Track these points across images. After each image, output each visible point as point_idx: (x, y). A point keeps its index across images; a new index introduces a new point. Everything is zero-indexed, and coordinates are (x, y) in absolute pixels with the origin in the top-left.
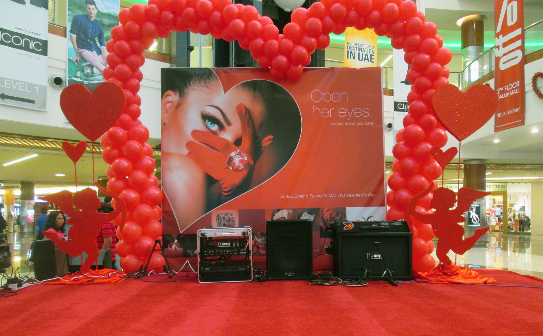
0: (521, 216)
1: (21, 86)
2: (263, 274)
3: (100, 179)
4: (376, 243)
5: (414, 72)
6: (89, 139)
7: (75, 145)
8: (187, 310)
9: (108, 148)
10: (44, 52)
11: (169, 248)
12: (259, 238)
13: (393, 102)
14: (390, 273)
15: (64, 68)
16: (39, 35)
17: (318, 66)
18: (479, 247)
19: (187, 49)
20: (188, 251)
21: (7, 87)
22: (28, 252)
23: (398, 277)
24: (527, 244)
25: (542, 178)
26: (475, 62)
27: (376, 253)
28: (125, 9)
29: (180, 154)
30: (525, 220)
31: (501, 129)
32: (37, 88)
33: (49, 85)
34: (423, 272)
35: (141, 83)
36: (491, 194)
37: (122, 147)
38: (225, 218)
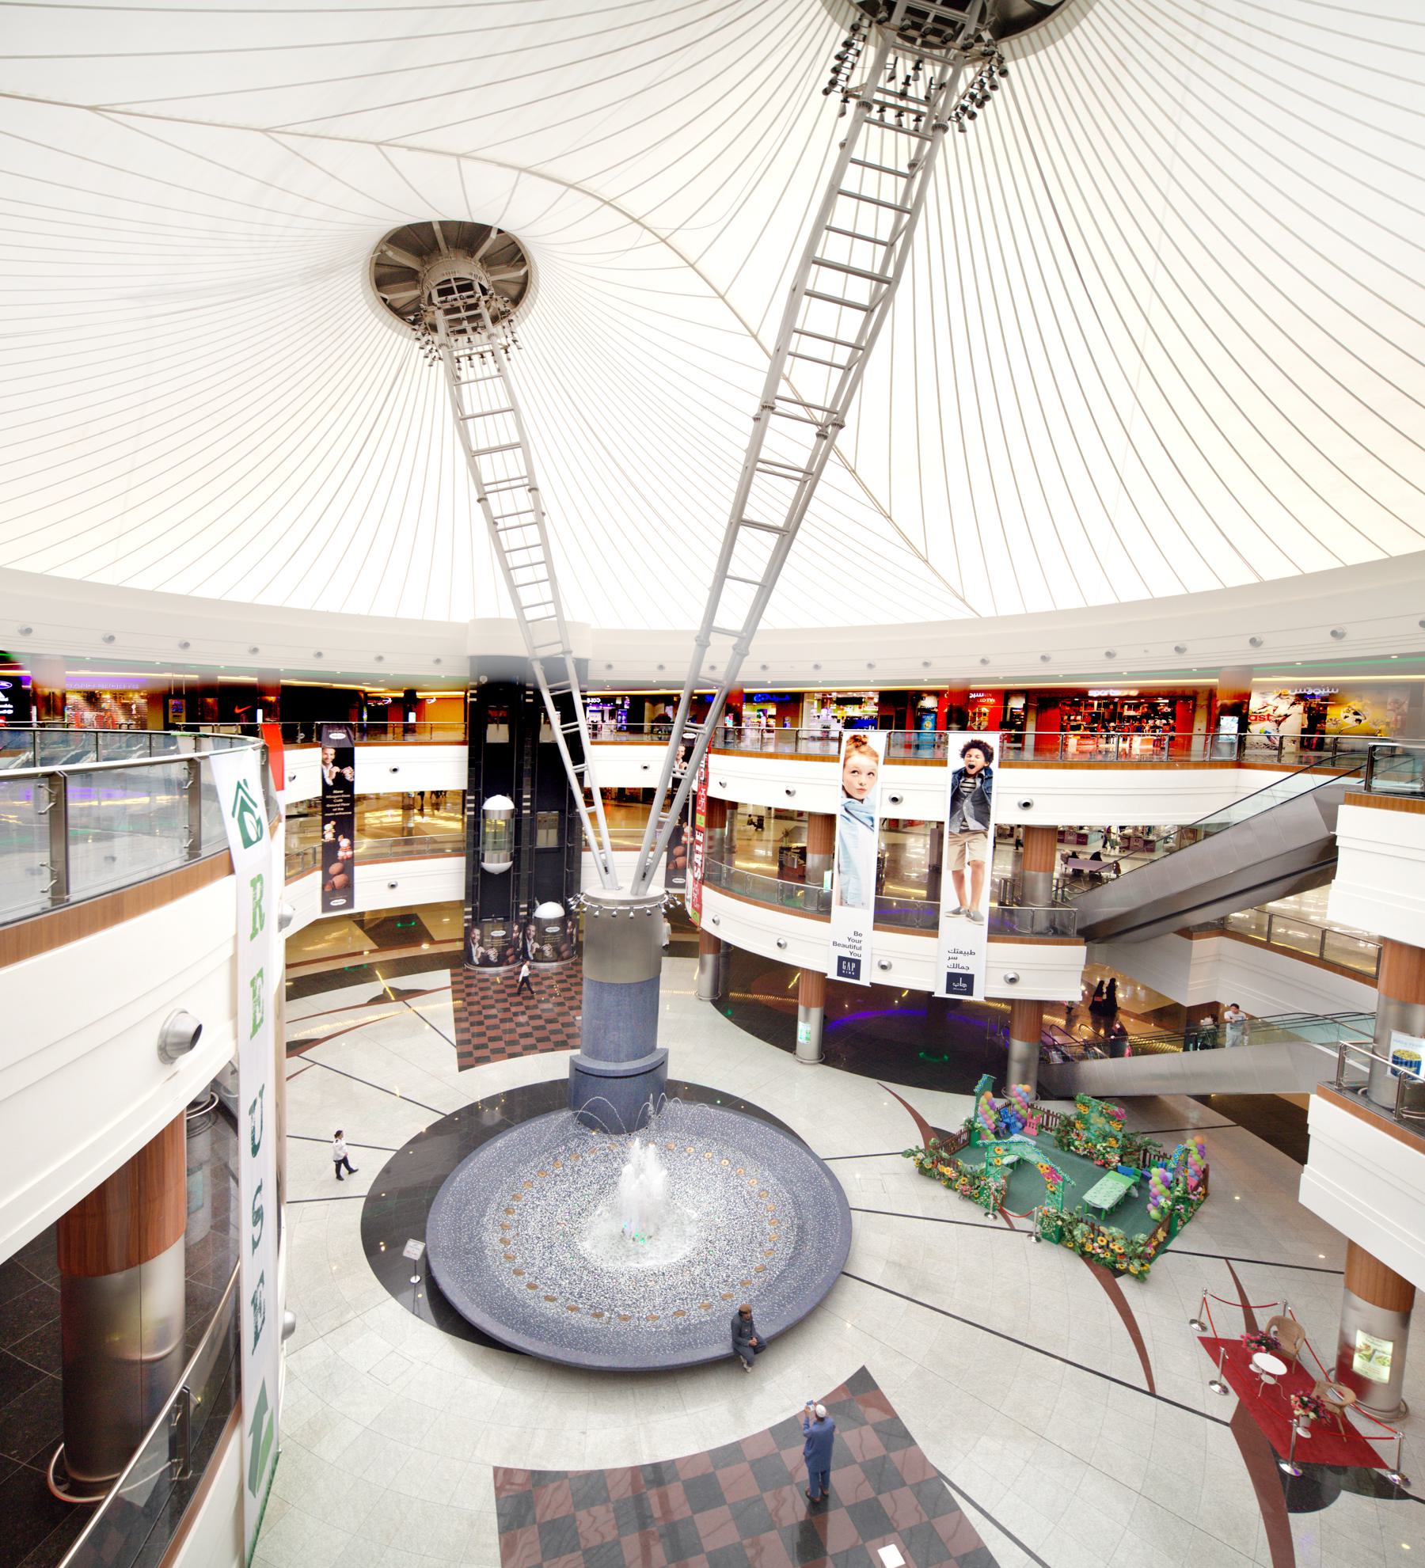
0: (1073, 1136)
1: (458, 284)
2: (981, 776)
3: (172, 748)
4: (733, 997)
5: (460, 1035)
6: (1232, 1120)
7: (544, 738)
8: (1099, 1251)
9: (131, 696)
10: (260, 877)
11: (705, 1521)
12: (1028, 755)
13: (859, 1367)
14: (154, 1353)
15: (1043, 28)
16: (262, 1280)
17: (769, 1435)
18: (1407, 810)
19: (1037, 1063)
20: (382, 1243)
21: (185, 1123)
22: (197, 1399)
23: (63, 1262)
24: (1030, 870)
25: (2, 803)
26: (728, 301)
27: (730, 1013)
28: (519, 1548)
29: (1371, 1334)
30: (524, 812)
31: (428, 854)
32: (393, 998)
33: (1124, 1176)
34: (28, 684)
35: (1082, 969)
36: (1346, 1361)
37: (1118, 1026)
38: (367, 828)
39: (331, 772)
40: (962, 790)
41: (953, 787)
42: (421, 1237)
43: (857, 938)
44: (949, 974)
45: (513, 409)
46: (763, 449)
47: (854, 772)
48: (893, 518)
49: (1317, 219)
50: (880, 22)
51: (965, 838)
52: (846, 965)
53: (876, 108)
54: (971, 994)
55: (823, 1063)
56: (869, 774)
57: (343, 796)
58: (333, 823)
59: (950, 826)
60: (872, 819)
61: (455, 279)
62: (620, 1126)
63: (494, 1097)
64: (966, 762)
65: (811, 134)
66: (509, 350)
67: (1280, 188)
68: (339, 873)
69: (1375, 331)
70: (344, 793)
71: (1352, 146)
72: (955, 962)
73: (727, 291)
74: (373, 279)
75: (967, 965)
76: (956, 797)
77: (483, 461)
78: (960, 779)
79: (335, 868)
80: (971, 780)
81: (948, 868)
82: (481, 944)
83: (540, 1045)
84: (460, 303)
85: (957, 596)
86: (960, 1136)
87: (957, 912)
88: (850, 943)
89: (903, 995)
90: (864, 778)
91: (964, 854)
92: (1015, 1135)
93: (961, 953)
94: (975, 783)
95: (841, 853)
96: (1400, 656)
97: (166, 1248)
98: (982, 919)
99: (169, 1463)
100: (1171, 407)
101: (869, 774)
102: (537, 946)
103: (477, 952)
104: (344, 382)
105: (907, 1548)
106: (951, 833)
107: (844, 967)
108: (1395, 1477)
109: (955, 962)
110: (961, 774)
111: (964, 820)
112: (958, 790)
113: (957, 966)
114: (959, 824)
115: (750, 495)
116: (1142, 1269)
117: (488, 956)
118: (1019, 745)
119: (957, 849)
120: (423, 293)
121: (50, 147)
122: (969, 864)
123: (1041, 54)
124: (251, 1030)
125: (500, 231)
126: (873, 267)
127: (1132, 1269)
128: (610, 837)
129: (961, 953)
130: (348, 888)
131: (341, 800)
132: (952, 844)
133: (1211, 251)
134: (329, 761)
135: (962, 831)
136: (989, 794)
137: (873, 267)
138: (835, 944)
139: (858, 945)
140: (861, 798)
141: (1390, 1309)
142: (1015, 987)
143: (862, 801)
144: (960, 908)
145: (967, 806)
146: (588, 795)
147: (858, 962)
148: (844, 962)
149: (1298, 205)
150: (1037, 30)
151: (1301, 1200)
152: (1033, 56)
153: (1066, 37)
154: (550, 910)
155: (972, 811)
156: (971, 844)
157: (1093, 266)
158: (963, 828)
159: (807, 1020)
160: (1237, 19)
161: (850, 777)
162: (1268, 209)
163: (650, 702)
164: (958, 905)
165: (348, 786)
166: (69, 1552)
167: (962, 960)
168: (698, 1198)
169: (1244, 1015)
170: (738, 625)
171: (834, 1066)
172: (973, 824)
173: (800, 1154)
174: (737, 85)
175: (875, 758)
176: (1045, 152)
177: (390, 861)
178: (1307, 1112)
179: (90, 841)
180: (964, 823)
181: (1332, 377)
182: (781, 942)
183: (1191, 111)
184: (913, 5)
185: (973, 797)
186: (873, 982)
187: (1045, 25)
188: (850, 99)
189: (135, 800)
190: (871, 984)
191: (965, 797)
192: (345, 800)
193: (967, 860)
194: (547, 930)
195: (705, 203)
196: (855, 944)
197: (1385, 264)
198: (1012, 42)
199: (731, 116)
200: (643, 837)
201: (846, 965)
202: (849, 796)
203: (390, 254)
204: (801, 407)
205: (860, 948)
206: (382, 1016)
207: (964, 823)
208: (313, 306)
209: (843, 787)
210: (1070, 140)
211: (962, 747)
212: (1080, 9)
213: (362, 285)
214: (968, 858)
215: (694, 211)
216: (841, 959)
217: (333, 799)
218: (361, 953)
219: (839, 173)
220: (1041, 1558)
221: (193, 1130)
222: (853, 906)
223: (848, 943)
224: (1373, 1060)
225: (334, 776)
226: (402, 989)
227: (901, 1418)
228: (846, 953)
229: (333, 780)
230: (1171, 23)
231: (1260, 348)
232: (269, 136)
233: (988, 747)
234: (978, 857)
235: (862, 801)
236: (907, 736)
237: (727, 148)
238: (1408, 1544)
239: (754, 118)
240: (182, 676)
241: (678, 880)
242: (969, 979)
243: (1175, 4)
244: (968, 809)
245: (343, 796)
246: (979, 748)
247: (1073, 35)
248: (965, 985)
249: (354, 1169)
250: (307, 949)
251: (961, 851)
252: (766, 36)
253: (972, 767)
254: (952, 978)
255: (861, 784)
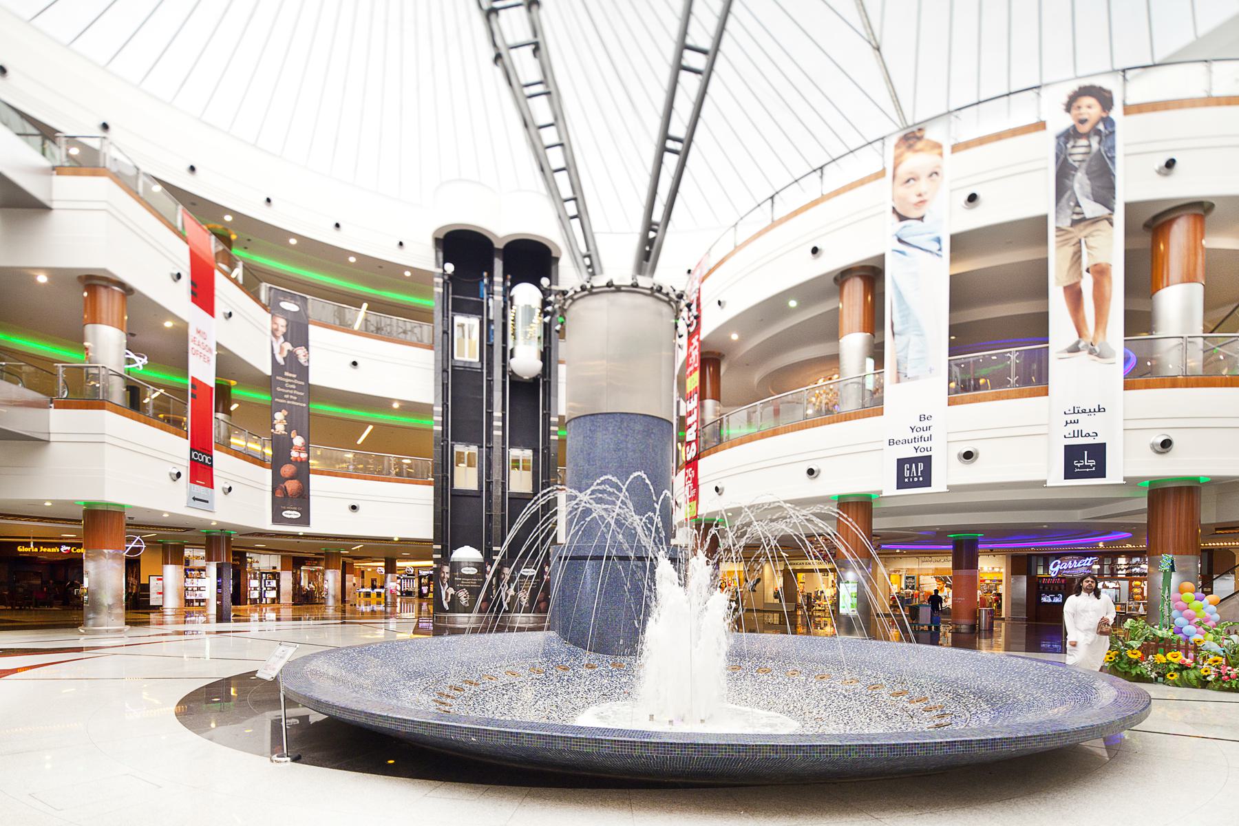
2: (1098, 133)
39: (282, 349)
40: (1070, 160)
41: (1057, 157)
42: (217, 726)
43: (925, 424)
44: (1066, 447)
47: (908, 181)
48: (882, 50)
49: (766, 30)
51: (1080, 232)
52: (910, 469)
54: (1104, 476)
56: (931, 175)
57: (296, 381)
58: (285, 412)
59: (1057, 218)
60: (938, 240)
61: (622, 501)
62: (584, 635)
64: (1075, 117)
68: (292, 478)
69: (97, 19)
70: (491, 276)
72: (1076, 427)
74: (1203, 200)
75: (1094, 429)
76: (1064, 172)
77: (687, 53)
78: (1066, 143)
79: (287, 470)
80: (1083, 142)
81: (1057, 284)
82: (452, 583)
87: (1075, 349)
88: (916, 434)
90: (923, 185)
91: (1080, 257)
92: (467, 548)
93: (1084, 411)
94: (1090, 146)
95: (895, 305)
97: (198, 733)
98: (1112, 354)
100: (138, 30)
101: (931, 175)
102: (451, 591)
103: (447, 594)
106: (1058, 229)
107: (907, 473)
109: (1076, 427)
110: (1070, 135)
111: (1078, 205)
112: (1066, 160)
113: (1080, 434)
114: (1069, 212)
116: (829, 624)
117: (296, 357)
118: (1209, 590)
119: (1069, 250)
120: (447, 612)
122: (1088, 271)
127: (725, 567)
129: (1084, 411)
130: (302, 500)
131: (294, 387)
132: (1061, 244)
133: (834, 58)
134: (279, 334)
135: (1074, 223)
136: (1112, 159)
138: (891, 442)
139: (926, 434)
140: (919, 214)
143: (921, 219)
144: (1078, 343)
145: (1080, 183)
146: (878, 615)
147: (927, 460)
148: (907, 466)
155: (1088, 189)
156: (1091, 241)
158: (1076, 217)
159: (498, 496)
161: (902, 191)
164: (1075, 337)
165: (303, 371)
166: (307, 269)
167: (1087, 424)
169: (829, 592)
171: (272, 739)
172: (1091, 209)
173: (442, 642)
174: (86, 29)
175: (937, 151)
177: (163, 223)
179: (213, 725)
180: (1078, 210)
181: (746, 8)
185: (1089, 166)
186: (1126, 475)
189: (763, 339)
190: (1125, 479)
191: (1076, 169)
192: (299, 388)
193: (1084, 267)
194: (299, 515)
196: (922, 433)
202: (902, 218)
205: (930, 438)
206: (244, 537)
207: (1078, 210)
208: (586, 40)
209: (894, 210)
211: (1065, 100)
214: (1086, 262)
216: (901, 463)
217: (285, 382)
221: (1077, 243)
222: (916, 378)
223: (910, 436)
224: (602, 558)
225: (285, 354)
228: (908, 452)
229: (285, 359)
231: (767, 30)
232: (881, 36)
233: (1104, 90)
234: (1101, 259)
235: (921, 219)
236: (378, 318)
238: (390, 764)
239: (731, 163)
242: (1098, 451)
244: (1082, 187)
245: (296, 381)
248: (1092, 463)
249: (880, 168)
251: (1075, 253)
253: (1083, 122)
254: (1072, 453)
255: (920, 195)
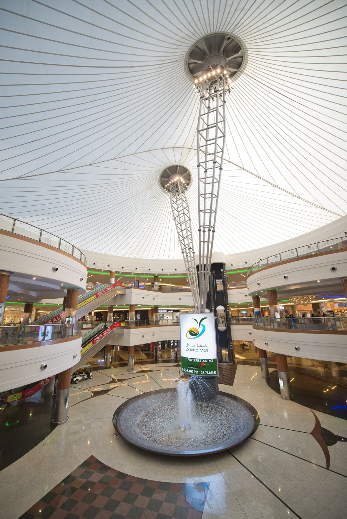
45: (267, 258)
46: (212, 179)
50: (240, 346)
52: (197, 372)
53: (108, 288)
55: (292, 400)
63: (285, 355)
65: (285, 18)
66: (230, 91)
67: (335, 471)
71: (319, 105)
73: (13, 228)
83: (225, 383)
84: (194, 276)
85: (295, 196)
86: (202, 82)
89: (324, 392)
96: (322, 281)
99: (258, 416)
104: (253, 67)
105: (169, 503)
108: (121, 504)
115: (216, 201)
121: (311, 131)
123: (241, 77)
124: (204, 320)
125: (180, 166)
126: (208, 213)
128: (233, 39)
137: (208, 213)
141: (283, 372)
142: (46, 370)
149: (319, 105)
150: (233, 78)
151: (338, 442)
152: (241, 76)
153: (240, 77)
154: (114, 318)
157: (314, 44)
160: (263, 24)
162: (333, 103)
163: (332, 377)
166: (94, 271)
168: (165, 402)
170: (208, 225)
176: (340, 147)
178: (40, 346)
182: (297, 347)
183: (273, 3)
184: (198, 46)
187: (210, 33)
188: (214, 98)
195: (56, 126)
197: (337, 137)
198: (225, 360)
199: (276, 107)
200: (196, 46)
201: (197, 372)
203: (162, 179)
204: (203, 121)
210: (144, 151)
212: (246, 62)
213: (184, 64)
215: (277, 86)
218: (205, 270)
219: (75, 259)
220: (118, 10)
224: (334, 318)
226: (335, 434)
227: (260, 272)
230: (257, 36)
237: (267, 100)
240: (138, 309)
241: (274, 309)
243: (164, 2)
246: (181, 174)
247: (249, 56)
250: (293, 378)
252: (320, 128)
254: (233, 341)
